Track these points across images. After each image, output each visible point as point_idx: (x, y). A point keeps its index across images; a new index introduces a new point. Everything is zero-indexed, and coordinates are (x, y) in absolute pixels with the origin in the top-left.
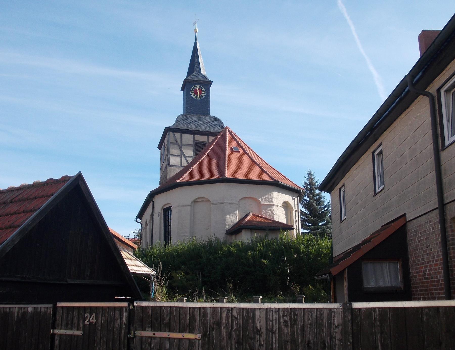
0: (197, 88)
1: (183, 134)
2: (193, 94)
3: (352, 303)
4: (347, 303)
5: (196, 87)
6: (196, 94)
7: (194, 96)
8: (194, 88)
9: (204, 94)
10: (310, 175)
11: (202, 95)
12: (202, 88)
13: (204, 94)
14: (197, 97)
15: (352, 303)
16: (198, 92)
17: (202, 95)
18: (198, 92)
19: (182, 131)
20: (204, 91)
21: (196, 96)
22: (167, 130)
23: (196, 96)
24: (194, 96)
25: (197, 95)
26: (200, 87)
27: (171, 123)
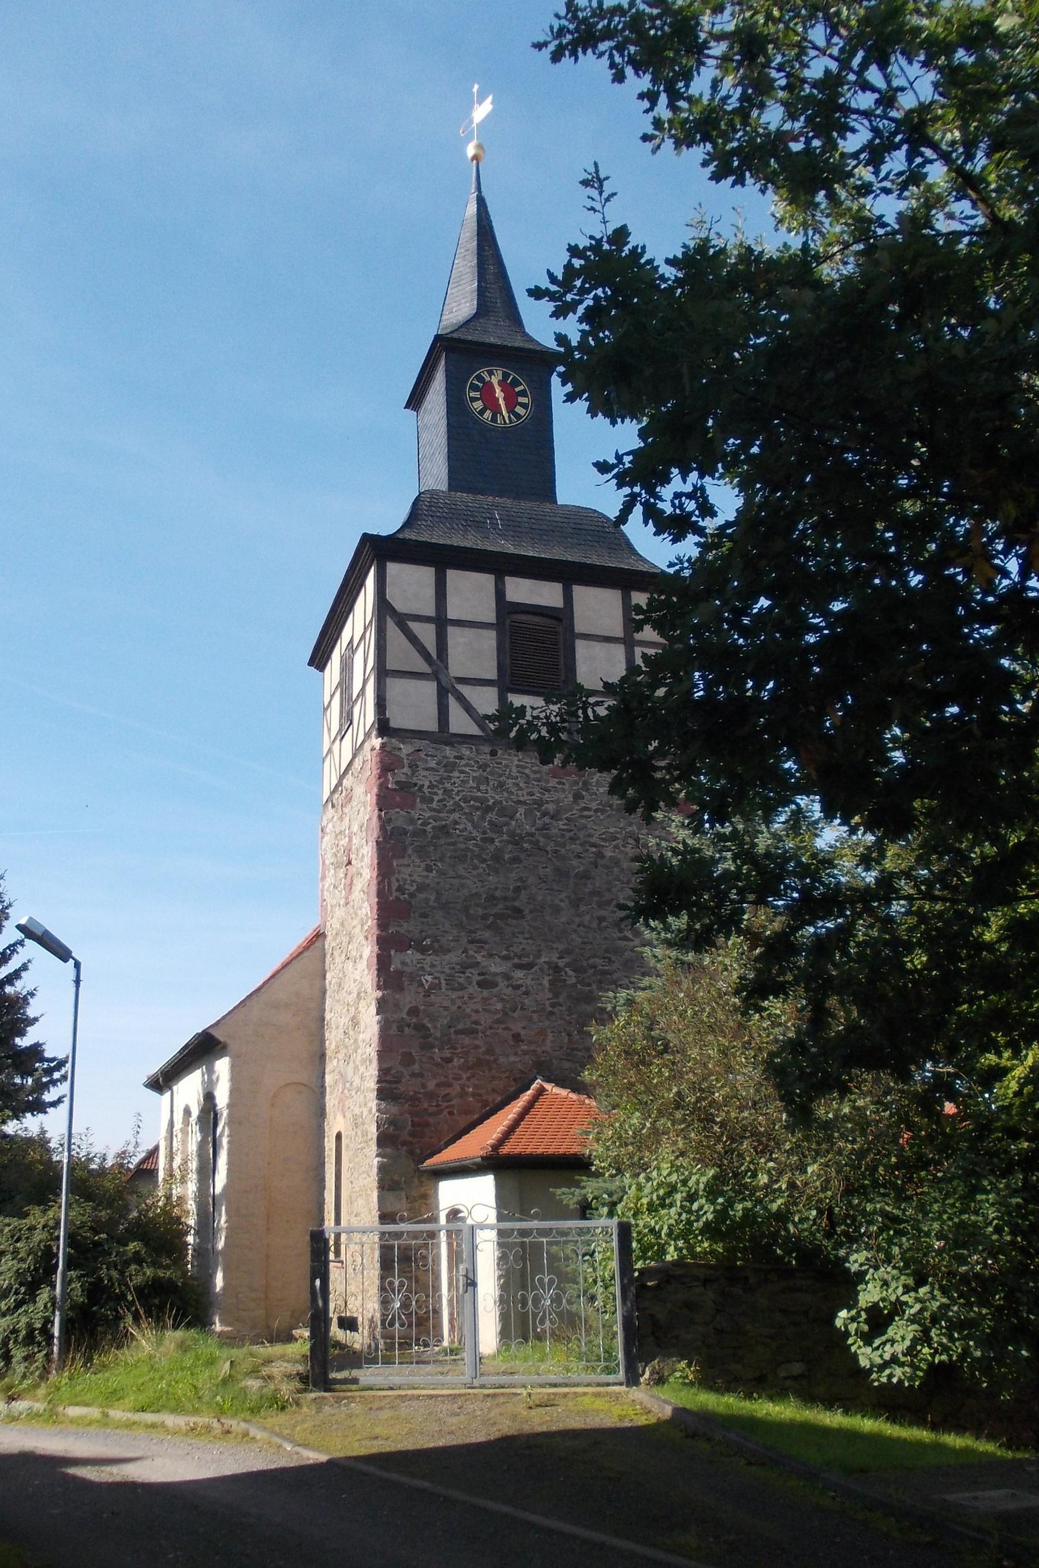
0: (495, 380)
1: (452, 575)
2: (478, 405)
3: (388, 564)
4: (909, 948)
5: (491, 373)
6: (491, 403)
7: (482, 412)
8: (480, 378)
9: (524, 406)
10: (603, 467)
11: (519, 410)
12: (515, 383)
13: (524, 406)
14: (494, 419)
15: (388, 564)
16: (499, 394)
17: (519, 410)
18: (499, 394)
19: (442, 559)
20: (523, 393)
21: (488, 414)
22: (376, 551)
23: (488, 414)
24: (482, 412)
25: (496, 411)
26: (505, 376)
27: (388, 521)
